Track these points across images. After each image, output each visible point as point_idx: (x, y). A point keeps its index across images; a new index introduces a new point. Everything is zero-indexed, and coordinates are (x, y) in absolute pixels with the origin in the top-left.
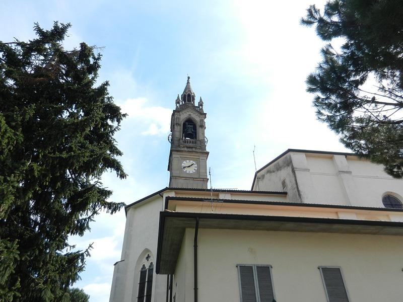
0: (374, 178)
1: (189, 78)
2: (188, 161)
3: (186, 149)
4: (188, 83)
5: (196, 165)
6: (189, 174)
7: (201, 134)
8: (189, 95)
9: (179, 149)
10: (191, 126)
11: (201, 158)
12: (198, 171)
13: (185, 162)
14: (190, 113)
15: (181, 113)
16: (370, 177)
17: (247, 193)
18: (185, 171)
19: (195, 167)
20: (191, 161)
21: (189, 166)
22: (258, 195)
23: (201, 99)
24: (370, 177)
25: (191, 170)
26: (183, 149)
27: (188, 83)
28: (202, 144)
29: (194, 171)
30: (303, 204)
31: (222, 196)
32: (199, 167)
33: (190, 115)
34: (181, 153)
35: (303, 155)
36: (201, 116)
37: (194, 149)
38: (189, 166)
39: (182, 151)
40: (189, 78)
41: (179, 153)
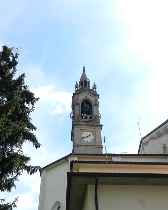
2: (86, 132)
3: (84, 123)
4: (84, 71)
5: (93, 136)
6: (88, 142)
7: (96, 111)
9: (79, 123)
10: (87, 105)
11: (96, 130)
12: (95, 140)
13: (84, 133)
14: (86, 95)
18: (84, 140)
20: (89, 133)
21: (88, 137)
25: (89, 140)
26: (82, 123)
27: (84, 71)
29: (92, 140)
32: (95, 137)
37: (90, 123)
38: (87, 136)
39: (81, 125)
40: (84, 68)
41: (79, 126)
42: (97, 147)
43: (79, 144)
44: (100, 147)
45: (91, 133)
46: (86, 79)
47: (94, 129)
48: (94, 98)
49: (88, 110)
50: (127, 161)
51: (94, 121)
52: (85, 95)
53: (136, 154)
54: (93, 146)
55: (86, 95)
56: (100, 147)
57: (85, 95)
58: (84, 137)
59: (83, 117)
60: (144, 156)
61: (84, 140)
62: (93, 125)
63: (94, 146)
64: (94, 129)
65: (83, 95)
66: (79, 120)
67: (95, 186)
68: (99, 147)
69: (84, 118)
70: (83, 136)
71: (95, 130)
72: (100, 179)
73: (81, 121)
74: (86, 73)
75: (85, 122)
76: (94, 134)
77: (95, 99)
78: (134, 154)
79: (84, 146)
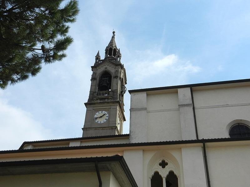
0: (223, 106)
1: (114, 33)
2: (100, 112)
3: (99, 101)
4: (113, 37)
5: (108, 115)
6: (101, 124)
7: (115, 84)
8: (115, 50)
9: (93, 102)
10: (106, 79)
11: (112, 107)
12: (108, 120)
13: (97, 114)
14: (107, 66)
15: (98, 68)
16: (218, 107)
17: (98, 139)
18: (96, 121)
19: (106, 117)
20: (104, 112)
21: (101, 117)
22: (111, 139)
23: (98, 53)
24: (218, 107)
25: (102, 121)
26: (96, 102)
27: (113, 37)
28: (115, 94)
29: (105, 121)
30: (133, 144)
31: (72, 145)
32: (109, 117)
33: (106, 68)
34: (94, 106)
35: (144, 94)
36: (117, 67)
37: (106, 100)
38: (102, 117)
39: (94, 104)
40: (114, 33)
41: (92, 106)
42: (95, 130)
43: (90, 127)
44: (113, 128)
45: (106, 113)
46: (112, 47)
47: (110, 107)
48: (115, 69)
49: (106, 85)
50: (113, 143)
51: (110, 98)
52: (105, 67)
53: (16, 149)
54: (104, 128)
55: (107, 66)
56: (113, 128)
57: (105, 67)
58: (96, 118)
59: (98, 94)
60: (110, 137)
61: (96, 121)
62: (108, 103)
63: (106, 127)
64: (110, 107)
65: (103, 67)
66: (93, 98)
67: (96, 173)
68: (112, 129)
69: (99, 95)
70: (96, 116)
71: (110, 108)
72: (100, 165)
73: (94, 99)
74: (116, 40)
75: (101, 99)
76: (109, 114)
77: (116, 69)
78: (9, 150)
79: (94, 129)
